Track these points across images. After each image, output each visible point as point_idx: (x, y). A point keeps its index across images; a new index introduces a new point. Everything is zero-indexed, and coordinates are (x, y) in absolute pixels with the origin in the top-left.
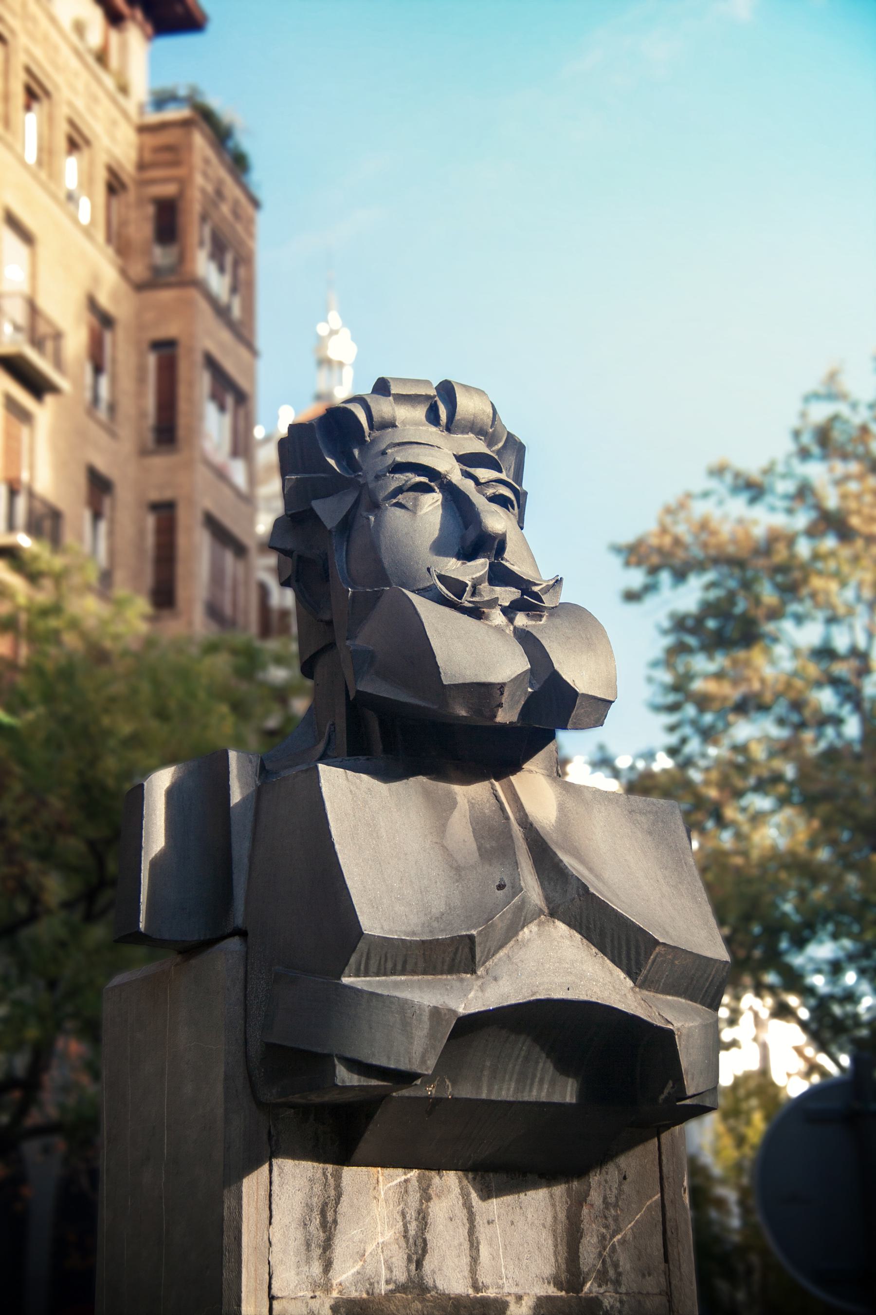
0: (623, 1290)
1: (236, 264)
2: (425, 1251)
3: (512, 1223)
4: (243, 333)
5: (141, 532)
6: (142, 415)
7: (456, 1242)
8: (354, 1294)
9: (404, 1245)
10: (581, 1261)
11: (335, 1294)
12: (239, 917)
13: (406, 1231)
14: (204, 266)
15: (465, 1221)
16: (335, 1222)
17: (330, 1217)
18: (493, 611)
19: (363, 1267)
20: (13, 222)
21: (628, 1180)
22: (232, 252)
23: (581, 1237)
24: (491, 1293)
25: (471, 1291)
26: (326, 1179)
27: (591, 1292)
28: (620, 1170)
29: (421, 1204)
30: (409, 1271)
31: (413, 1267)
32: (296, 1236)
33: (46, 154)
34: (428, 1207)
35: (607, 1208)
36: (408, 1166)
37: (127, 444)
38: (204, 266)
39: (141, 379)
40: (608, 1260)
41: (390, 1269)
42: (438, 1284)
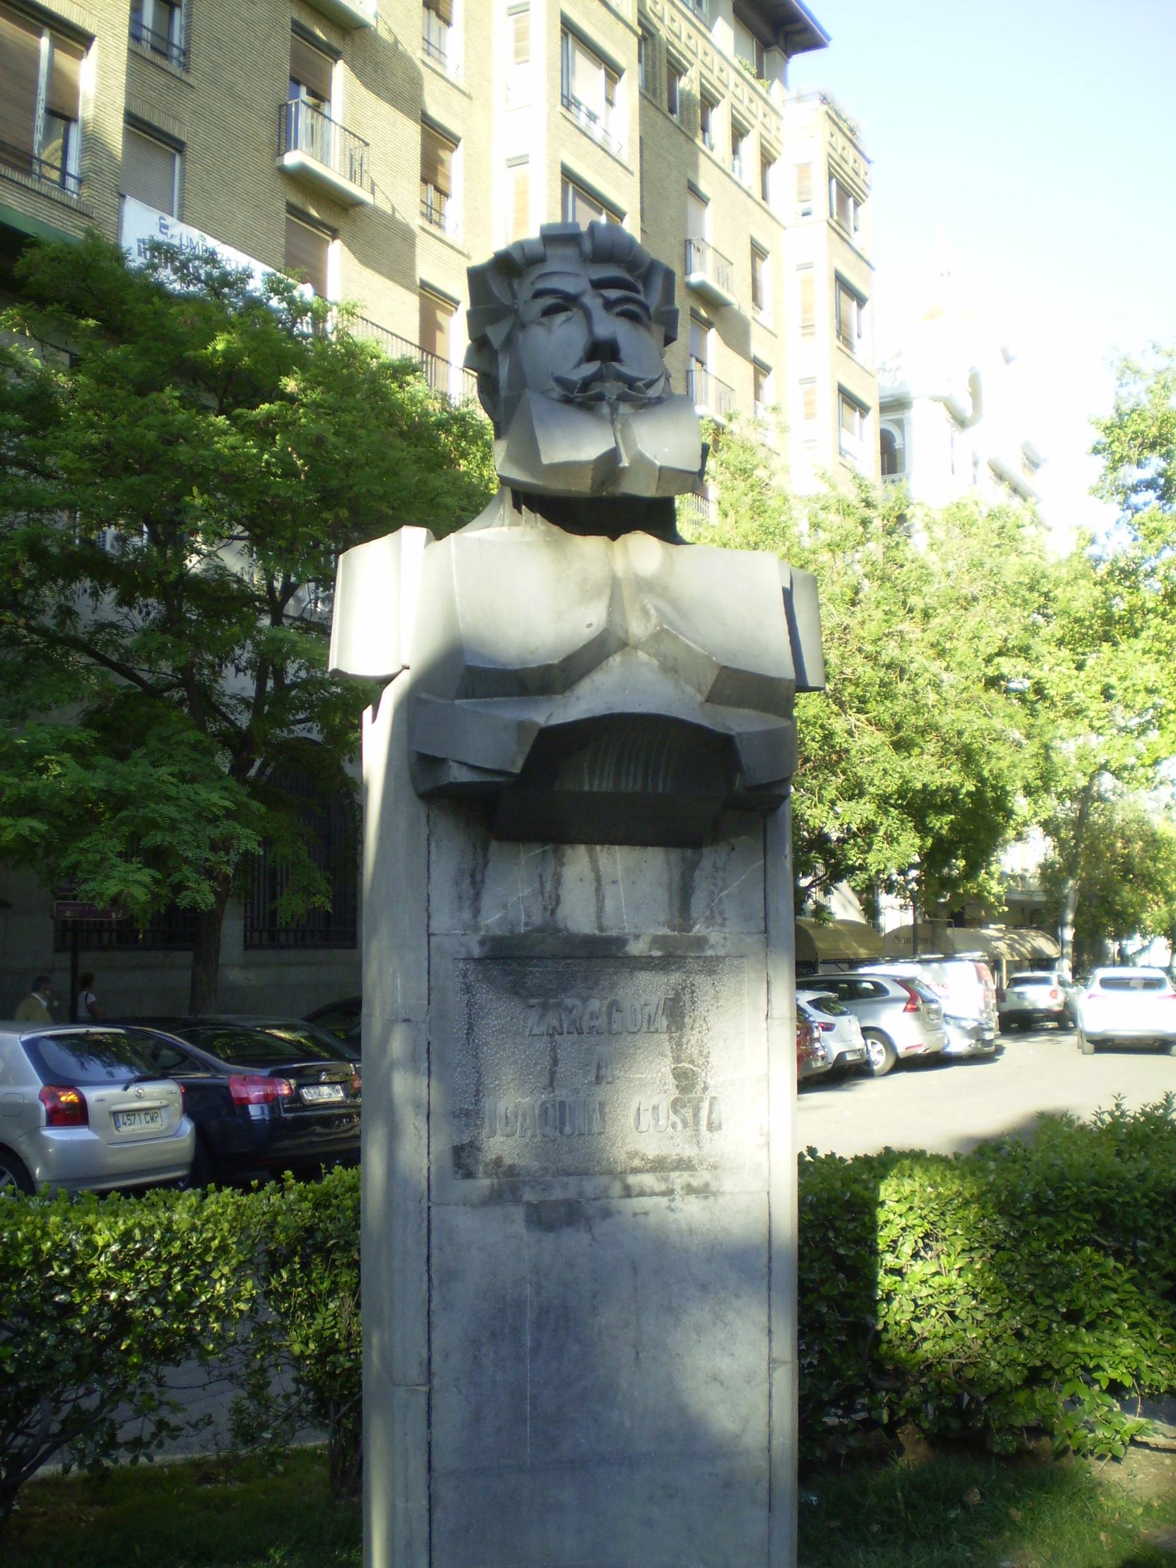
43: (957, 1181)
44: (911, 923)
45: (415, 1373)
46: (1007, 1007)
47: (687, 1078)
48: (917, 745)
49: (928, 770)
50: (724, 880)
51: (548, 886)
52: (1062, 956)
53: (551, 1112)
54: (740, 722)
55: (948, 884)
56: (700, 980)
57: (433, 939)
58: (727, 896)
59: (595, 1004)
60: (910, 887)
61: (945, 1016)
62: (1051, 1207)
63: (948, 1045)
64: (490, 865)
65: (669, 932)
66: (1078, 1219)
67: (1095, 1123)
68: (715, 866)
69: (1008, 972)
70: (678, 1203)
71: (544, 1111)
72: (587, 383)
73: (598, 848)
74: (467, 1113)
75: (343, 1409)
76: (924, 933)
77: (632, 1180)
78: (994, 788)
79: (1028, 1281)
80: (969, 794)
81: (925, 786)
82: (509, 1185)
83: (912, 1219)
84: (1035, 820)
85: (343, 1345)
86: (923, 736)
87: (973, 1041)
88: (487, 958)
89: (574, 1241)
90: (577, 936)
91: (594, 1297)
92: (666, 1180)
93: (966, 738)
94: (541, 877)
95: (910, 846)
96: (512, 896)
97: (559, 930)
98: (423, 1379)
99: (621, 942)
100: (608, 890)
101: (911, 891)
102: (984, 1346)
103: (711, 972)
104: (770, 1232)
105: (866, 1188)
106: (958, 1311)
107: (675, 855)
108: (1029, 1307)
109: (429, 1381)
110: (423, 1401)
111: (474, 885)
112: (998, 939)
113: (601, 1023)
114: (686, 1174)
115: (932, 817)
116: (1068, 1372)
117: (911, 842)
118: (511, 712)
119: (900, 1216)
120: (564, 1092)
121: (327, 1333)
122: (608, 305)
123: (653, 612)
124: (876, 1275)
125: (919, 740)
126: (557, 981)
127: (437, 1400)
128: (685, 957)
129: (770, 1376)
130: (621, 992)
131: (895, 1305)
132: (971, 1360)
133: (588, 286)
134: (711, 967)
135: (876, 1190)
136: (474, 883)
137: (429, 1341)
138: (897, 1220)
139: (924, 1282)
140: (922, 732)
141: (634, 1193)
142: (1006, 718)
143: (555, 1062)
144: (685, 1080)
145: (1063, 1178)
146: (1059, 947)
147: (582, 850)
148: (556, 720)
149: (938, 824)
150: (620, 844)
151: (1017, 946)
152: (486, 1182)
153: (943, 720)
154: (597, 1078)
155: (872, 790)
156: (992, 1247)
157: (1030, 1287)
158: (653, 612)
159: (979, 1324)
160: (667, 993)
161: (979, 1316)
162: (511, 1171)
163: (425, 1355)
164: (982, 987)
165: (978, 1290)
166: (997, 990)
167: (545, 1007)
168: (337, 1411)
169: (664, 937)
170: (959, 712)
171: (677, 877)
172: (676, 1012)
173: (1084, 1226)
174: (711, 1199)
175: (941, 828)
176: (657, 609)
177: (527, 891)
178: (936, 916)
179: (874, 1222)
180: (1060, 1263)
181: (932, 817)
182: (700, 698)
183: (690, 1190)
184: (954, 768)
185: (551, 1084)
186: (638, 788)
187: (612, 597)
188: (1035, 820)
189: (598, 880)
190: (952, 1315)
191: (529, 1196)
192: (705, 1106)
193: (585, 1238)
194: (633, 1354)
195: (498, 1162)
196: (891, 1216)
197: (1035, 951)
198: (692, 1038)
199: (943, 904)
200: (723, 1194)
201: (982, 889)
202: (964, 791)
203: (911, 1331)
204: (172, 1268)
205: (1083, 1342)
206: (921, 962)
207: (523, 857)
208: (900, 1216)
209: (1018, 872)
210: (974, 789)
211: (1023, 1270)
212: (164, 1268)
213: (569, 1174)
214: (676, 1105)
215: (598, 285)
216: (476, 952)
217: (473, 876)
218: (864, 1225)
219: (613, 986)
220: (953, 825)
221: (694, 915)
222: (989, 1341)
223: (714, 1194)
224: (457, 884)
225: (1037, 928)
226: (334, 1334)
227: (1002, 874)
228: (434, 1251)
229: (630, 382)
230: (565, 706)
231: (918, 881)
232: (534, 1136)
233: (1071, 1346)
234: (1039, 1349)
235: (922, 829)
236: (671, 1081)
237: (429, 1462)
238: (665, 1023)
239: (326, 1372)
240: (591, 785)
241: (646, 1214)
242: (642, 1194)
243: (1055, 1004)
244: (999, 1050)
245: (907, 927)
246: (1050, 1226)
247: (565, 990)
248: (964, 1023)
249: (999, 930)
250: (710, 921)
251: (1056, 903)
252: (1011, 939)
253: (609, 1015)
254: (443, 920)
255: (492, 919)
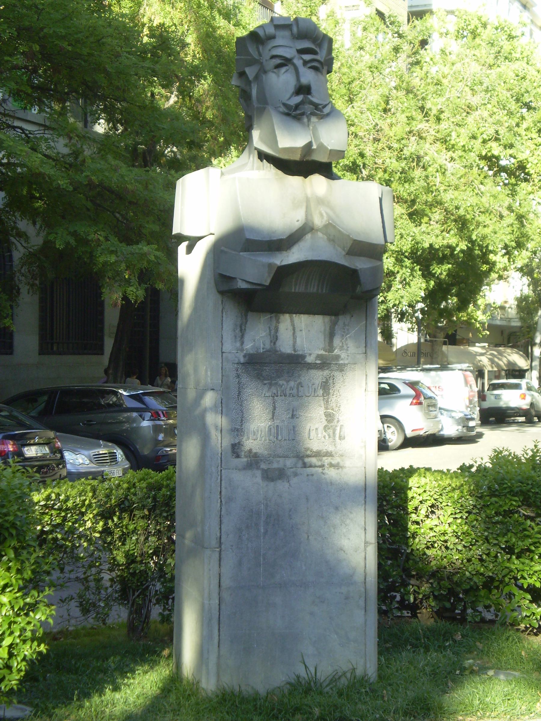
43: (448, 480)
44: (416, 341)
45: (214, 543)
46: (486, 405)
47: (330, 416)
48: (427, 215)
49: (433, 234)
50: (348, 330)
51: (273, 332)
52: (531, 368)
53: (273, 431)
54: (361, 264)
55: (447, 313)
56: (336, 374)
57: (224, 354)
58: (350, 337)
59: (292, 384)
60: (416, 315)
61: (440, 409)
62: (497, 493)
63: (442, 430)
64: (248, 323)
65: (324, 353)
66: (511, 500)
67: (523, 455)
68: (344, 323)
69: (490, 379)
70: (326, 471)
71: (270, 430)
73: (294, 315)
74: (238, 429)
75: (136, 594)
76: (426, 349)
77: (307, 460)
78: (481, 247)
79: (485, 531)
80: (462, 251)
81: (431, 245)
82: (254, 461)
83: (425, 496)
84: (512, 267)
85: (139, 559)
86: (430, 209)
87: (460, 427)
88: (246, 363)
89: (282, 486)
90: (285, 354)
91: (290, 511)
92: (321, 460)
93: (462, 212)
94: (269, 328)
95: (419, 287)
96: (257, 337)
97: (277, 351)
98: (217, 546)
99: (303, 357)
100: (298, 334)
101: (417, 318)
102: (462, 563)
103: (342, 371)
104: (365, 485)
105: (402, 481)
106: (448, 544)
107: (327, 318)
108: (486, 545)
109: (220, 546)
110: (217, 555)
111: (241, 331)
112: (482, 354)
113: (295, 391)
114: (330, 458)
115: (435, 265)
116: (507, 579)
117: (419, 285)
118: (265, 259)
119: (419, 495)
120: (278, 421)
121: (132, 552)
123: (324, 214)
124: (407, 524)
125: (428, 211)
126: (278, 372)
127: (223, 555)
128: (330, 364)
129: (365, 549)
130: (303, 379)
131: (417, 540)
132: (456, 571)
134: (341, 368)
135: (407, 482)
136: (241, 330)
137: (220, 528)
138: (418, 497)
139: (431, 529)
140: (431, 206)
141: (308, 466)
142: (493, 192)
143: (275, 408)
144: (330, 417)
145: (503, 479)
146: (529, 362)
147: (287, 316)
148: (284, 263)
149: (439, 271)
150: (304, 314)
151: (496, 360)
152: (245, 459)
153: (447, 197)
154: (292, 415)
155: (393, 248)
156: (466, 512)
157: (486, 534)
158: (324, 214)
159: (460, 551)
160: (322, 379)
161: (460, 547)
162: (256, 455)
163: (219, 535)
164: (468, 389)
165: (459, 534)
166: (479, 392)
167: (271, 385)
168: (134, 595)
169: (321, 355)
170: (456, 193)
171: (328, 328)
172: (326, 387)
173: (514, 503)
174: (340, 469)
175: (441, 274)
176: (327, 213)
177: (264, 334)
178: (435, 337)
179: (407, 497)
180: (501, 523)
181: (435, 265)
182: (344, 253)
183: (331, 465)
184: (452, 232)
185: (273, 418)
186: (315, 290)
187: (307, 207)
188: (512, 267)
189: (294, 329)
190: (447, 548)
191: (263, 466)
192: (338, 429)
193: (287, 485)
194: (306, 537)
195: (250, 451)
196: (415, 495)
197: (510, 363)
198: (333, 399)
199: (441, 327)
200: (345, 467)
201: (470, 317)
202: (458, 249)
203: (425, 554)
204: (67, 514)
205: (514, 563)
206: (423, 370)
207: (262, 319)
208: (419, 495)
209: (498, 304)
210: (465, 248)
211: (482, 525)
212: (63, 514)
213: (280, 457)
214: (326, 428)
216: (242, 360)
217: (241, 327)
218: (401, 499)
219: (299, 376)
220: (450, 273)
221: (335, 345)
222: (465, 561)
223: (342, 467)
224: (234, 331)
225: (513, 347)
226: (134, 553)
227: (488, 306)
228: (223, 489)
230: (288, 256)
231: (422, 311)
232: (265, 440)
233: (508, 565)
234: (491, 566)
235: (427, 274)
236: (324, 418)
237: (220, 583)
238: (321, 392)
239: (130, 573)
240: (295, 289)
241: (312, 475)
242: (311, 466)
243: (524, 404)
244: (480, 435)
245: (413, 344)
246: (496, 502)
247: (279, 377)
248: (453, 414)
249: (483, 347)
250: (341, 348)
251: (528, 327)
252: (492, 354)
253: (298, 389)
254: (228, 346)
255: (249, 346)
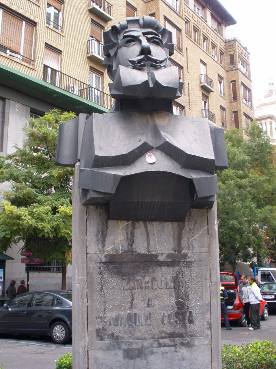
0: (195, 251)
1: (246, 65)
2: (133, 242)
3: (160, 235)
4: (248, 78)
5: (232, 117)
6: (230, 95)
7: (143, 240)
8: (112, 253)
9: (127, 241)
10: (182, 244)
11: (106, 253)
12: (79, 158)
13: (127, 237)
14: (240, 67)
15: (146, 234)
16: (106, 235)
17: (104, 233)
18: (145, 68)
19: (114, 246)
20: (202, 62)
21: (197, 223)
22: (245, 63)
23: (182, 238)
24: (154, 253)
25: (147, 253)
26: (103, 224)
27: (185, 252)
28: (195, 220)
29: (132, 230)
30: (128, 247)
31: (130, 246)
32: (94, 239)
33: (208, 48)
34: (134, 231)
35: (190, 230)
36: (128, 220)
37: (227, 101)
38: (240, 67)
39: (229, 88)
40: (190, 244)
41: (122, 247)
42: (137, 250)
72: (140, 61)
122: (149, 40)
133: (141, 34)
215: (144, 34)
229: (155, 61)
